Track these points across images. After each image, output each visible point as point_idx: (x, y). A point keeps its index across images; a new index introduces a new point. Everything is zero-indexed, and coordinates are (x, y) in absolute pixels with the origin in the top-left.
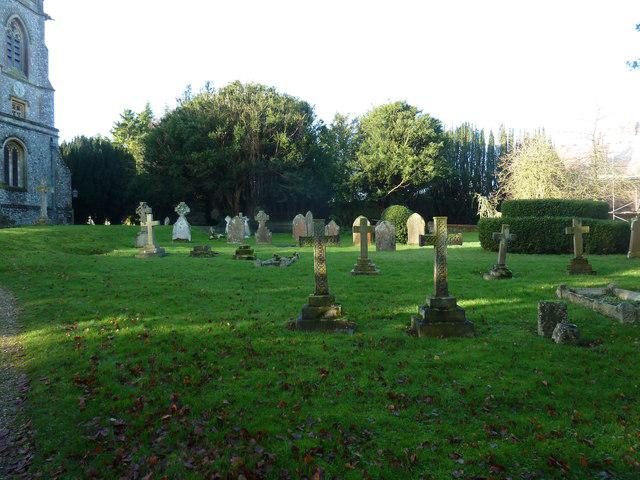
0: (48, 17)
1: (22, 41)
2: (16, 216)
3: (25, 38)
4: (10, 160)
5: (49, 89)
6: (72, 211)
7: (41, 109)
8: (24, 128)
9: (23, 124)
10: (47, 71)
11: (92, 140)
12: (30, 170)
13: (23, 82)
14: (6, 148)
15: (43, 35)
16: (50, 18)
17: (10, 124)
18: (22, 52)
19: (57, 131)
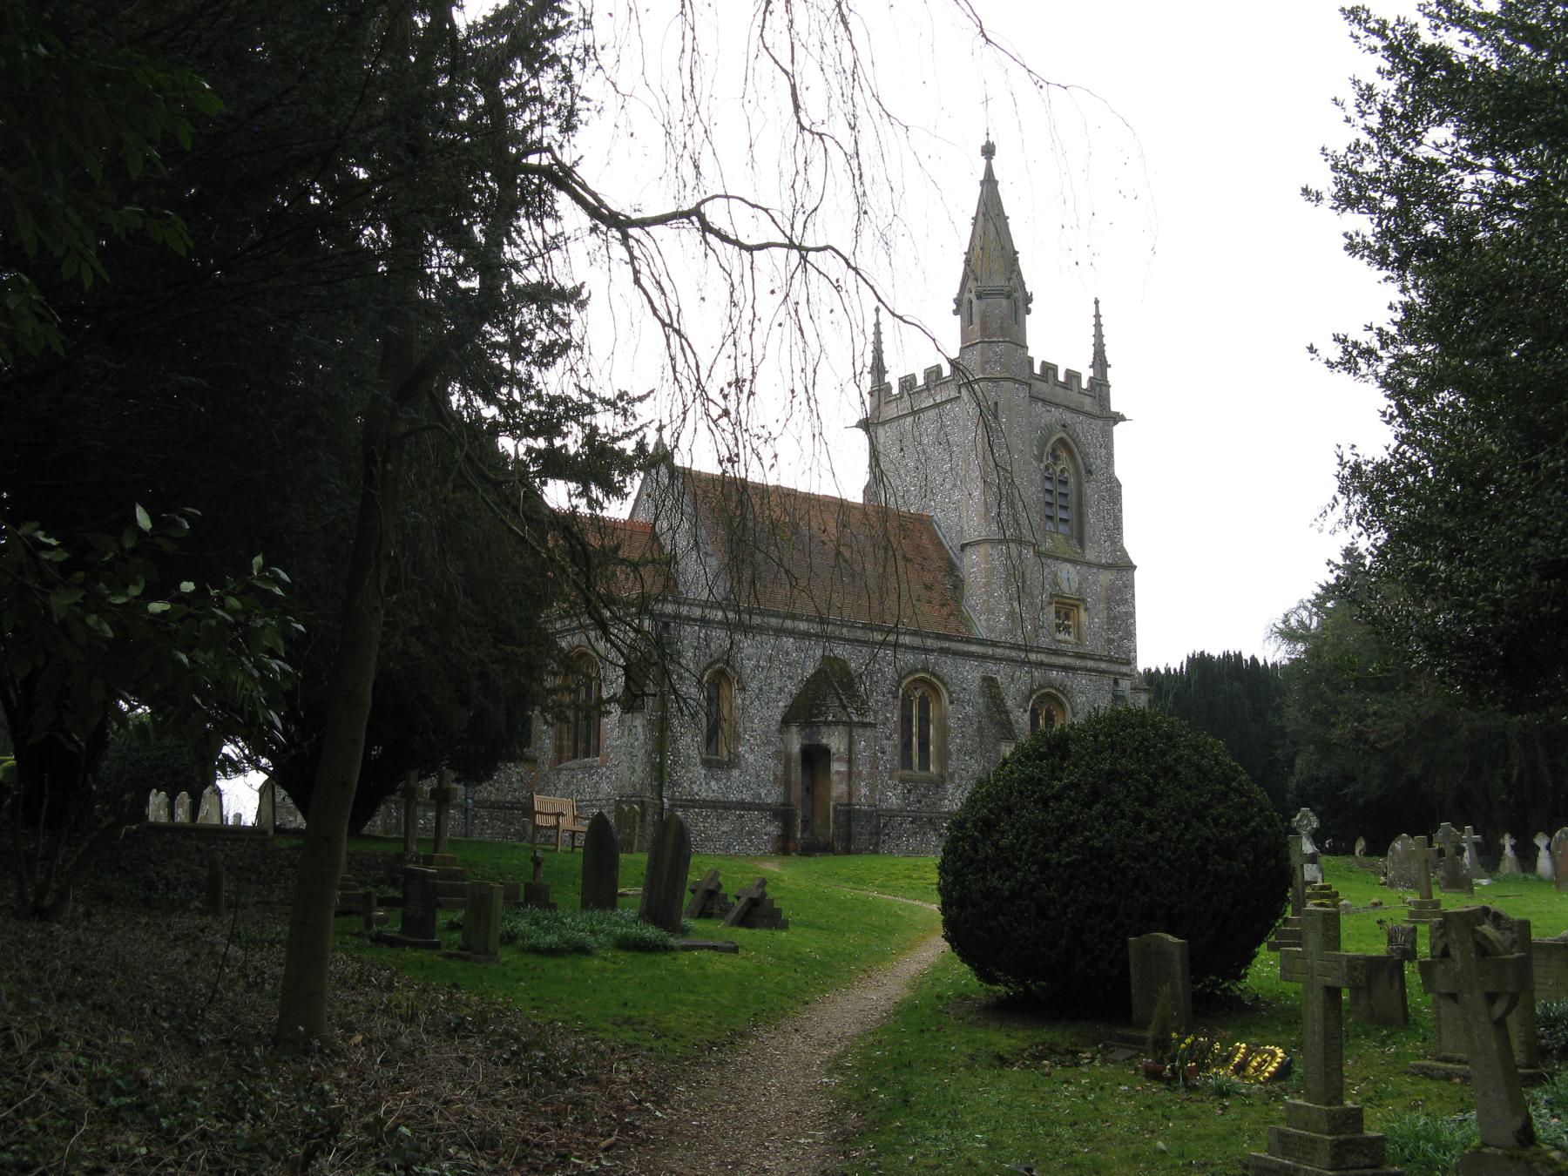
0: (1118, 418)
5: (1125, 567)
7: (1110, 609)
8: (1065, 668)
10: (1121, 534)
13: (1073, 562)
14: (1034, 711)
15: (1110, 456)
16: (1122, 418)
18: (1073, 499)
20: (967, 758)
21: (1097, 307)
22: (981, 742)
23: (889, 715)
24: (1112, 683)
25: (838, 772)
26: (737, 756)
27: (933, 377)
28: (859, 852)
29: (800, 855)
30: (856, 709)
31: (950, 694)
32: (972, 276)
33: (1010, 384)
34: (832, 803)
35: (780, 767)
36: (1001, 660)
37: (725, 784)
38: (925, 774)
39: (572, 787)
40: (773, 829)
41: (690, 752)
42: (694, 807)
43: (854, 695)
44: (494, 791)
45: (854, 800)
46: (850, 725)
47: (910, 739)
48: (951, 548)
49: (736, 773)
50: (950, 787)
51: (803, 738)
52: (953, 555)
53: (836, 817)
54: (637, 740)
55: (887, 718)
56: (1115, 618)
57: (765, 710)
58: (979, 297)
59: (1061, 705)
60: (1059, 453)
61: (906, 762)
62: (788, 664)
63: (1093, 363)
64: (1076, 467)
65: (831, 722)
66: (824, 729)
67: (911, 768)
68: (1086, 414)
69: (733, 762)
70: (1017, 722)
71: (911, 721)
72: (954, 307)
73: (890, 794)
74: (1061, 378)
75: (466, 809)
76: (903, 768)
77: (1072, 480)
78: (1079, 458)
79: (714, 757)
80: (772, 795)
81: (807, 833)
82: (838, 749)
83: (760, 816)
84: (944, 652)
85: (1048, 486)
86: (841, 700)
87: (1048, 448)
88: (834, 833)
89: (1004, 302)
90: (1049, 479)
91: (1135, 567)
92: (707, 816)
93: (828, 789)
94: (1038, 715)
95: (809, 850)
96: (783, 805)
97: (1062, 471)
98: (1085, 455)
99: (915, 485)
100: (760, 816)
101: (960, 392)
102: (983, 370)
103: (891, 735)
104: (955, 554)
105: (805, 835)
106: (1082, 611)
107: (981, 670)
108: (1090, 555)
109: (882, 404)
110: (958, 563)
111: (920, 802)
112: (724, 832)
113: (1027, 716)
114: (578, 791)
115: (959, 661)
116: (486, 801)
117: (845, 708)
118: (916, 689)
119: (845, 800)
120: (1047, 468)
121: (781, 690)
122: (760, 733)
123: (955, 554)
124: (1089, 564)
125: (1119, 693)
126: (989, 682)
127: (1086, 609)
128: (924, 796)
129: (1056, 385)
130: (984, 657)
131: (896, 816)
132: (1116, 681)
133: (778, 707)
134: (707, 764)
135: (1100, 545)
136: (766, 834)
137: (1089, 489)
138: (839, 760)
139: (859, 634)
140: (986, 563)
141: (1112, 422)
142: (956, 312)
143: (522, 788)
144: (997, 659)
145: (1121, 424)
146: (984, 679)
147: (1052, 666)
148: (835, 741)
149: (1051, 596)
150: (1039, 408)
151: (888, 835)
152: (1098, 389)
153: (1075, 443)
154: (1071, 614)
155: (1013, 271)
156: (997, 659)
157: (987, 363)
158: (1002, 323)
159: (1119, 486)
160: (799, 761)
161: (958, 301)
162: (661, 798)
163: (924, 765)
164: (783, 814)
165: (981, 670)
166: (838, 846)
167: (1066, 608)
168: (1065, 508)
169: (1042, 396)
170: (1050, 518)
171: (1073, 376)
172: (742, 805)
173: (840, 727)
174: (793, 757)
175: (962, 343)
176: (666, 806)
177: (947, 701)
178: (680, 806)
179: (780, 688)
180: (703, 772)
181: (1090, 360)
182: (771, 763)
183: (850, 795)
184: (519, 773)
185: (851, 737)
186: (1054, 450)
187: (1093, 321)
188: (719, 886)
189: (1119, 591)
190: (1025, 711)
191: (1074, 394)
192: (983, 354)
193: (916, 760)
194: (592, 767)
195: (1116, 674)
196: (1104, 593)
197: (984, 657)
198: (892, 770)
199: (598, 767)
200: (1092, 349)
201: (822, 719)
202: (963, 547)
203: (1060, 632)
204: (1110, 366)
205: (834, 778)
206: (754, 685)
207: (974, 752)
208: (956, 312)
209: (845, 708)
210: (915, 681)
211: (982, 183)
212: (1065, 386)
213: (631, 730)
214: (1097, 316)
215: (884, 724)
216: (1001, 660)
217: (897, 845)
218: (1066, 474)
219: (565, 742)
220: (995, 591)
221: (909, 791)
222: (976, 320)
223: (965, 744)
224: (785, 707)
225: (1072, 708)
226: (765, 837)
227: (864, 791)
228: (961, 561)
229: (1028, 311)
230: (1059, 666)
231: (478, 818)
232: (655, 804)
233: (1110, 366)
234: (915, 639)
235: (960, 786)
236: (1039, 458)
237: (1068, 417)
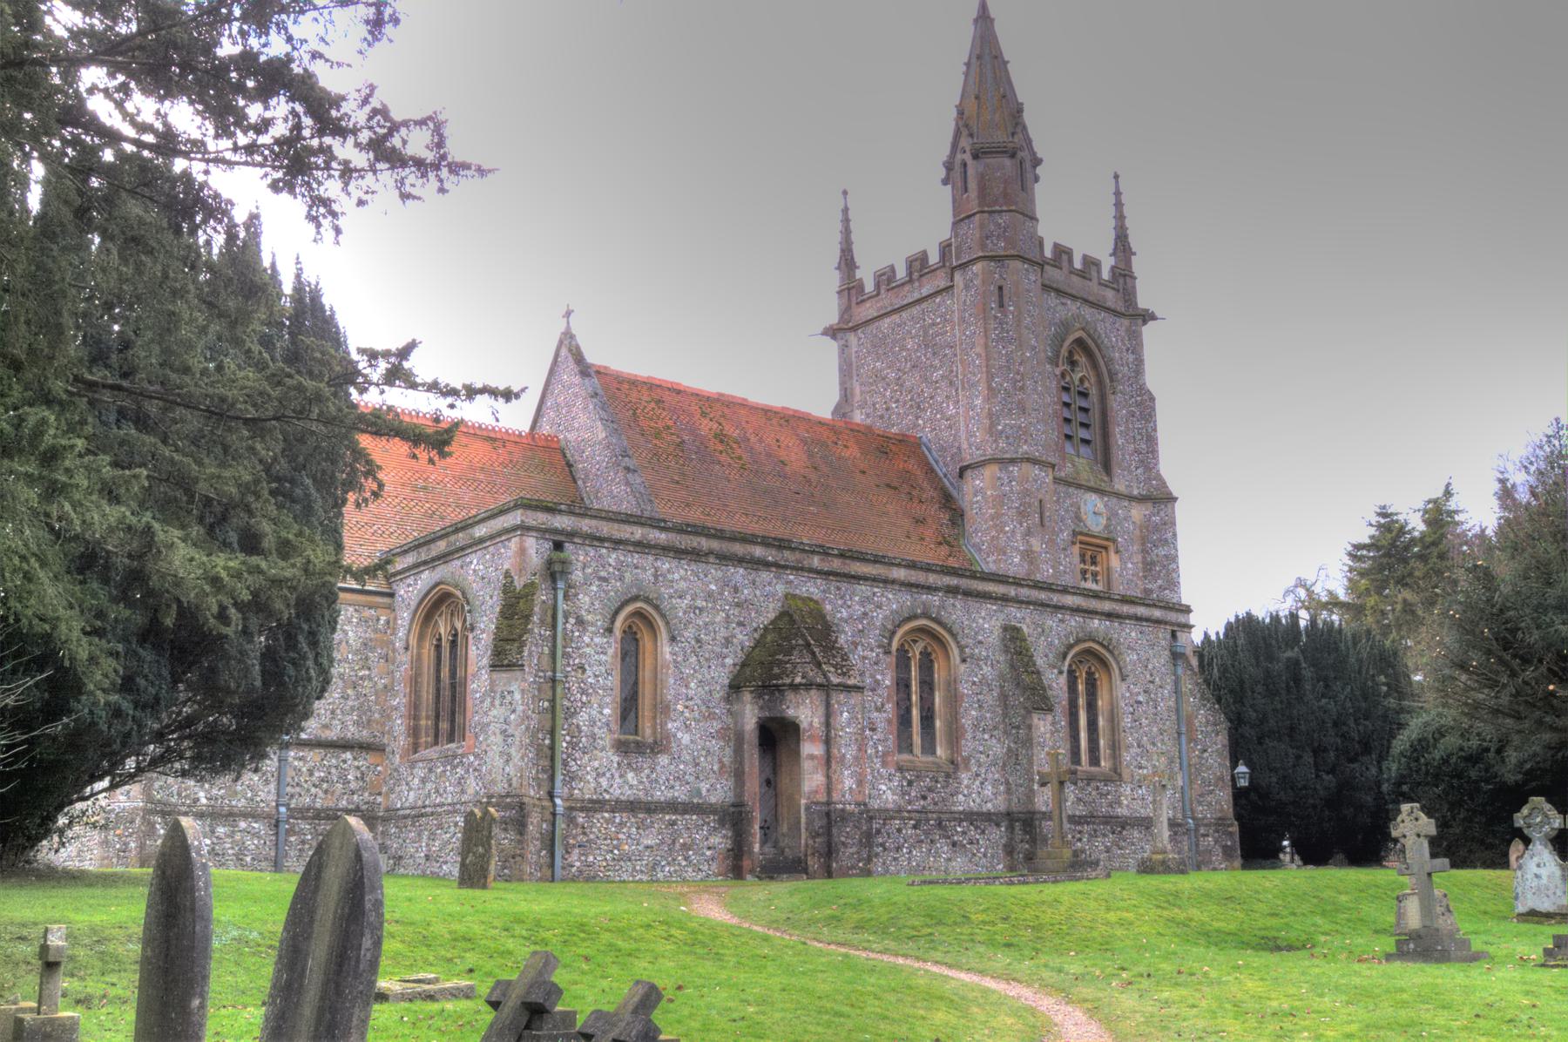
0: (1147, 317)
1: (1094, 392)
2: (1097, 847)
3: (1100, 383)
4: (1082, 701)
5: (1162, 498)
6: (1235, 829)
7: (1145, 551)
8: (1110, 616)
9: (1107, 606)
10: (1156, 458)
11: (1275, 619)
12: (1127, 721)
14: (1071, 672)
15: (1139, 362)
16: (1153, 317)
17: (1076, 610)
18: (1095, 417)
19: (1187, 610)
20: (986, 736)
21: (1117, 182)
22: (1005, 715)
23: (879, 677)
24: (1169, 636)
25: (812, 757)
26: (668, 737)
27: (917, 265)
28: (845, 873)
29: (760, 878)
30: (835, 666)
31: (961, 648)
32: (965, 132)
33: (1018, 264)
34: (803, 801)
35: (728, 751)
37: (648, 777)
38: (931, 759)
39: (429, 786)
40: (720, 840)
41: (596, 730)
42: (601, 810)
43: (830, 647)
44: (321, 794)
45: (836, 797)
46: (826, 688)
47: (908, 710)
48: (945, 476)
49: (663, 760)
50: (965, 777)
51: (761, 708)
52: (947, 483)
53: (809, 823)
54: (514, 711)
55: (877, 682)
56: (1153, 563)
57: (705, 670)
58: (976, 157)
59: (1104, 663)
60: (1076, 357)
61: (905, 744)
62: (738, 605)
63: (1115, 249)
64: (1099, 375)
65: (800, 684)
66: (790, 696)
67: (911, 752)
68: (1108, 309)
69: (658, 746)
70: (1051, 688)
71: (908, 686)
72: (942, 173)
73: (884, 788)
74: (1078, 264)
75: (278, 821)
76: (900, 751)
79: (631, 738)
80: (717, 791)
81: (769, 845)
82: (811, 724)
83: (700, 822)
84: (952, 591)
85: (1066, 398)
86: (813, 654)
87: (1064, 352)
88: (807, 845)
89: (1007, 162)
90: (1066, 389)
91: (1175, 499)
92: (622, 824)
93: (797, 781)
94: (1076, 678)
95: (781, 867)
96: (733, 805)
97: (1082, 380)
98: (1109, 362)
99: (897, 401)
100: (700, 822)
101: (952, 280)
102: (983, 246)
103: (883, 705)
104: (952, 484)
105: (766, 849)
106: (1112, 554)
107: (1002, 616)
108: (1120, 485)
109: (853, 304)
110: (954, 493)
111: (924, 798)
112: (647, 847)
113: (1063, 679)
114: (437, 791)
115: (971, 602)
116: (308, 810)
117: (819, 665)
118: (915, 641)
119: (822, 798)
120: (1063, 375)
121: (728, 641)
122: (699, 702)
123: (952, 484)
124: (1118, 495)
125: (1179, 650)
126: (1012, 635)
127: (1117, 552)
128: (930, 790)
129: (1071, 272)
131: (893, 818)
132: (1174, 635)
133: (723, 665)
134: (622, 747)
135: (1130, 472)
136: (709, 848)
137: (1116, 404)
138: (812, 738)
139: (836, 564)
140: (994, 487)
141: (1140, 322)
142: (945, 182)
143: (363, 789)
144: (1022, 602)
145: (1151, 323)
146: (1006, 629)
148: (805, 711)
149: (1075, 533)
150: (1052, 300)
151: (882, 845)
152: (1121, 280)
153: (1098, 346)
154: (1099, 559)
155: (1017, 124)
156: (1022, 602)
157: (987, 238)
158: (1005, 188)
159: (1152, 399)
160: (756, 741)
161: (949, 166)
162: (551, 796)
163: (929, 748)
164: (734, 817)
165: (1002, 616)
166: (814, 863)
167: (1093, 549)
168: (1085, 425)
169: (1055, 285)
170: (1068, 437)
171: (1091, 263)
172: (673, 807)
173: (813, 692)
174: (747, 736)
175: (954, 216)
176: (560, 810)
177: (958, 659)
178: (582, 809)
179: (726, 639)
180: (616, 759)
181: (1110, 247)
182: (715, 745)
183: (829, 790)
184: (358, 768)
185: (828, 705)
186: (1070, 353)
188: (555, 992)
189: (1156, 529)
190: (1061, 672)
191: (1094, 285)
192: (982, 226)
193: (917, 739)
194: (455, 757)
195: (1172, 624)
196: (1137, 532)
197: (1005, 599)
198: (885, 754)
199: (463, 756)
200: (1112, 235)
201: (788, 681)
202: (962, 472)
203: (1085, 580)
204: (1134, 254)
205: (807, 765)
206: (689, 633)
207: (995, 728)
208: (945, 182)
209: (819, 665)
210: (913, 630)
211: (976, 21)
212: (1083, 274)
213: (504, 697)
214: (1118, 194)
215: (873, 690)
217: (895, 859)
218: (1086, 384)
219: (423, 722)
220: (1006, 524)
221: (910, 783)
222: (973, 185)
223: (983, 718)
224: (735, 665)
225: (1120, 669)
226: (708, 853)
227: (848, 782)
228: (959, 490)
229: (1037, 179)
230: (1102, 614)
231: (295, 833)
232: (543, 808)
233: (1134, 254)
234: (913, 572)
235: (978, 775)
236: (1054, 361)
237: (1088, 312)
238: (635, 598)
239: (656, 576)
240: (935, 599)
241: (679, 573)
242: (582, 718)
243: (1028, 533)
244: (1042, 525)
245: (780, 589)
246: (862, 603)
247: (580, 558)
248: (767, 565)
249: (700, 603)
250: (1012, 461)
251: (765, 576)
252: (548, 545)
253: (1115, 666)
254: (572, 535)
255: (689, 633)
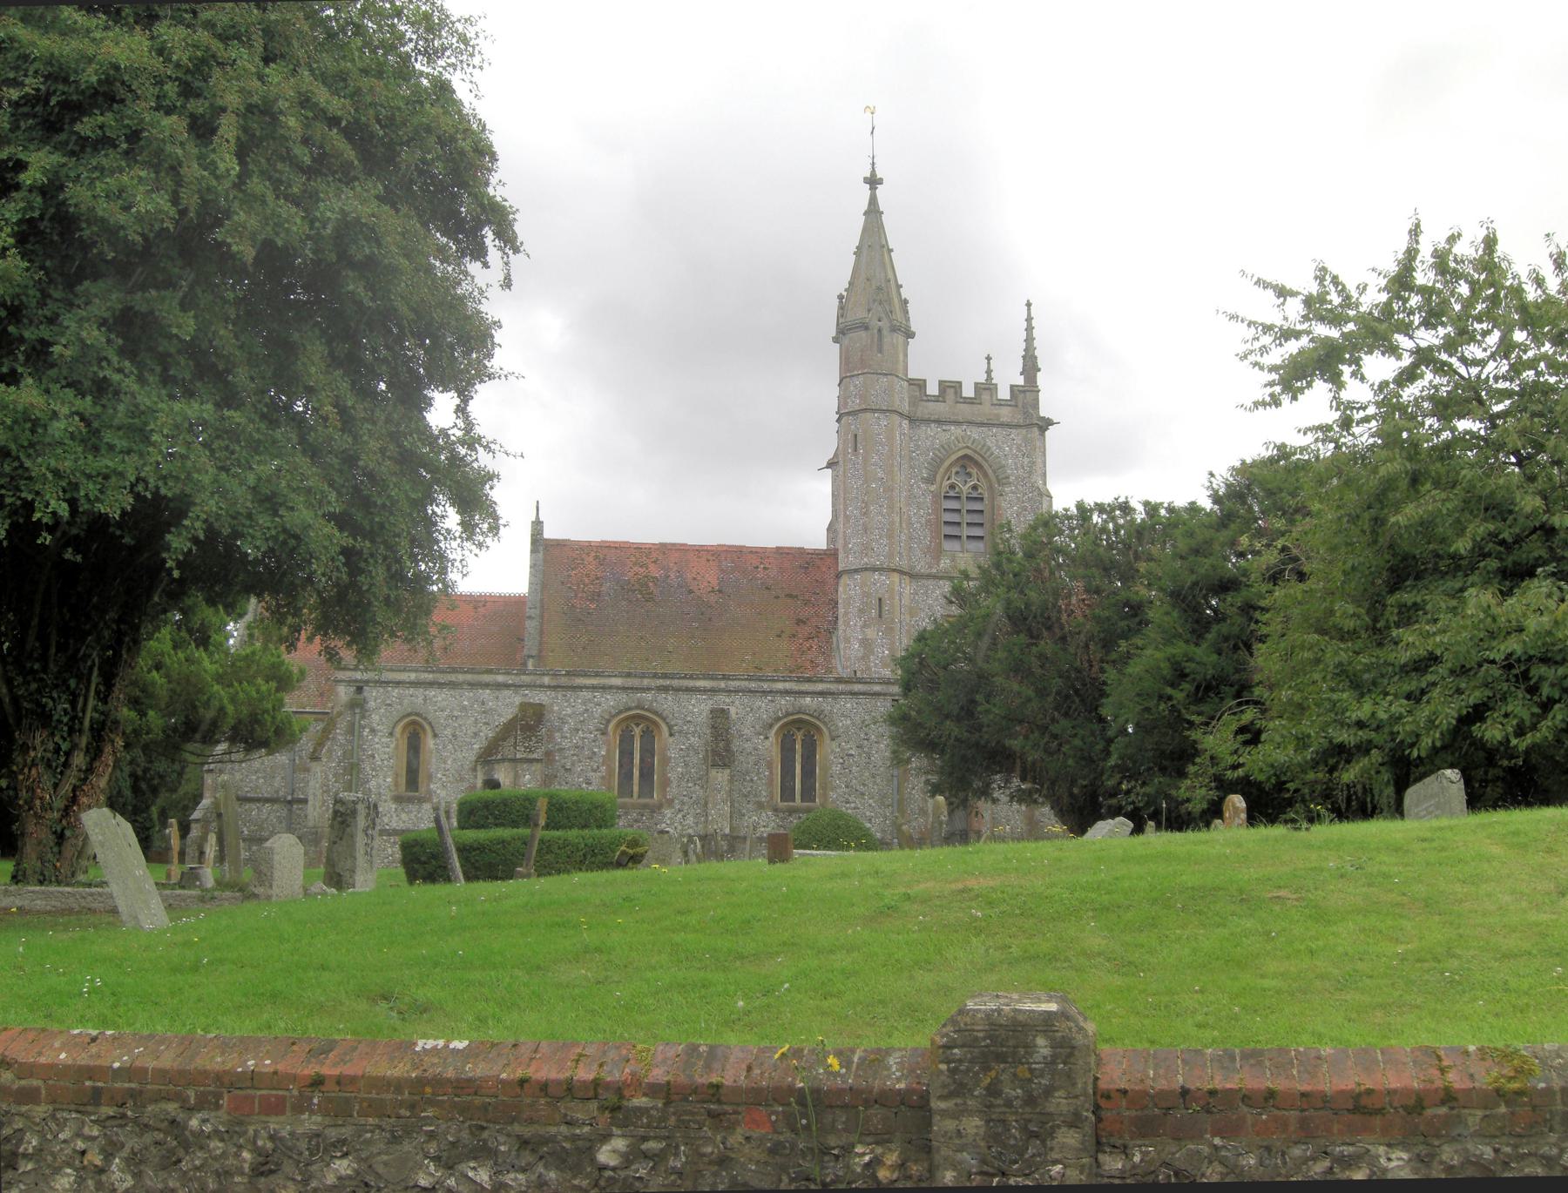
3: (991, 487)
8: (822, 694)
17: (787, 692)
21: (1029, 310)
31: (670, 727)
33: (868, 415)
36: (736, 691)
55: (594, 753)
59: (818, 729)
61: (787, 793)
77: (986, 496)
78: (990, 472)
84: (665, 689)
89: (863, 334)
115: (683, 696)
121: (476, 734)
126: (719, 715)
128: (636, 821)
130: (713, 691)
142: (836, 340)
147: (807, 693)
187: (1025, 325)
197: (713, 691)
214: (1029, 319)
216: (736, 691)
236: (930, 480)
237: (974, 433)
238: (409, 715)
239: (425, 700)
240: (649, 696)
241: (440, 697)
242: (373, 783)
243: (865, 626)
244: (880, 616)
245: (518, 700)
246: (584, 703)
247: (373, 695)
248: (507, 686)
249: (456, 713)
250: (856, 571)
251: (507, 692)
252: (353, 689)
253: (825, 729)
254: (367, 682)
255: (448, 732)
